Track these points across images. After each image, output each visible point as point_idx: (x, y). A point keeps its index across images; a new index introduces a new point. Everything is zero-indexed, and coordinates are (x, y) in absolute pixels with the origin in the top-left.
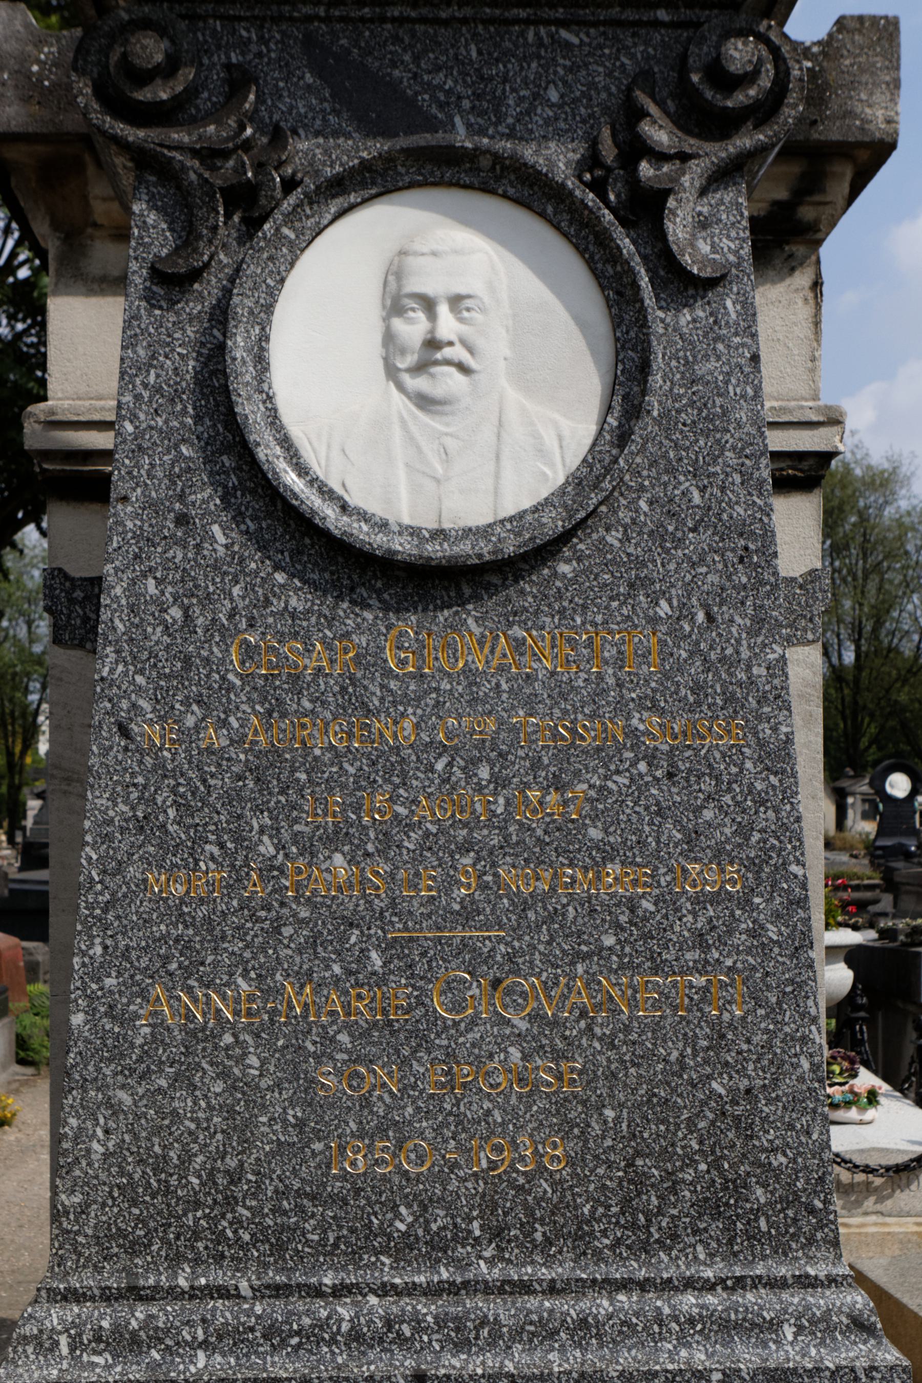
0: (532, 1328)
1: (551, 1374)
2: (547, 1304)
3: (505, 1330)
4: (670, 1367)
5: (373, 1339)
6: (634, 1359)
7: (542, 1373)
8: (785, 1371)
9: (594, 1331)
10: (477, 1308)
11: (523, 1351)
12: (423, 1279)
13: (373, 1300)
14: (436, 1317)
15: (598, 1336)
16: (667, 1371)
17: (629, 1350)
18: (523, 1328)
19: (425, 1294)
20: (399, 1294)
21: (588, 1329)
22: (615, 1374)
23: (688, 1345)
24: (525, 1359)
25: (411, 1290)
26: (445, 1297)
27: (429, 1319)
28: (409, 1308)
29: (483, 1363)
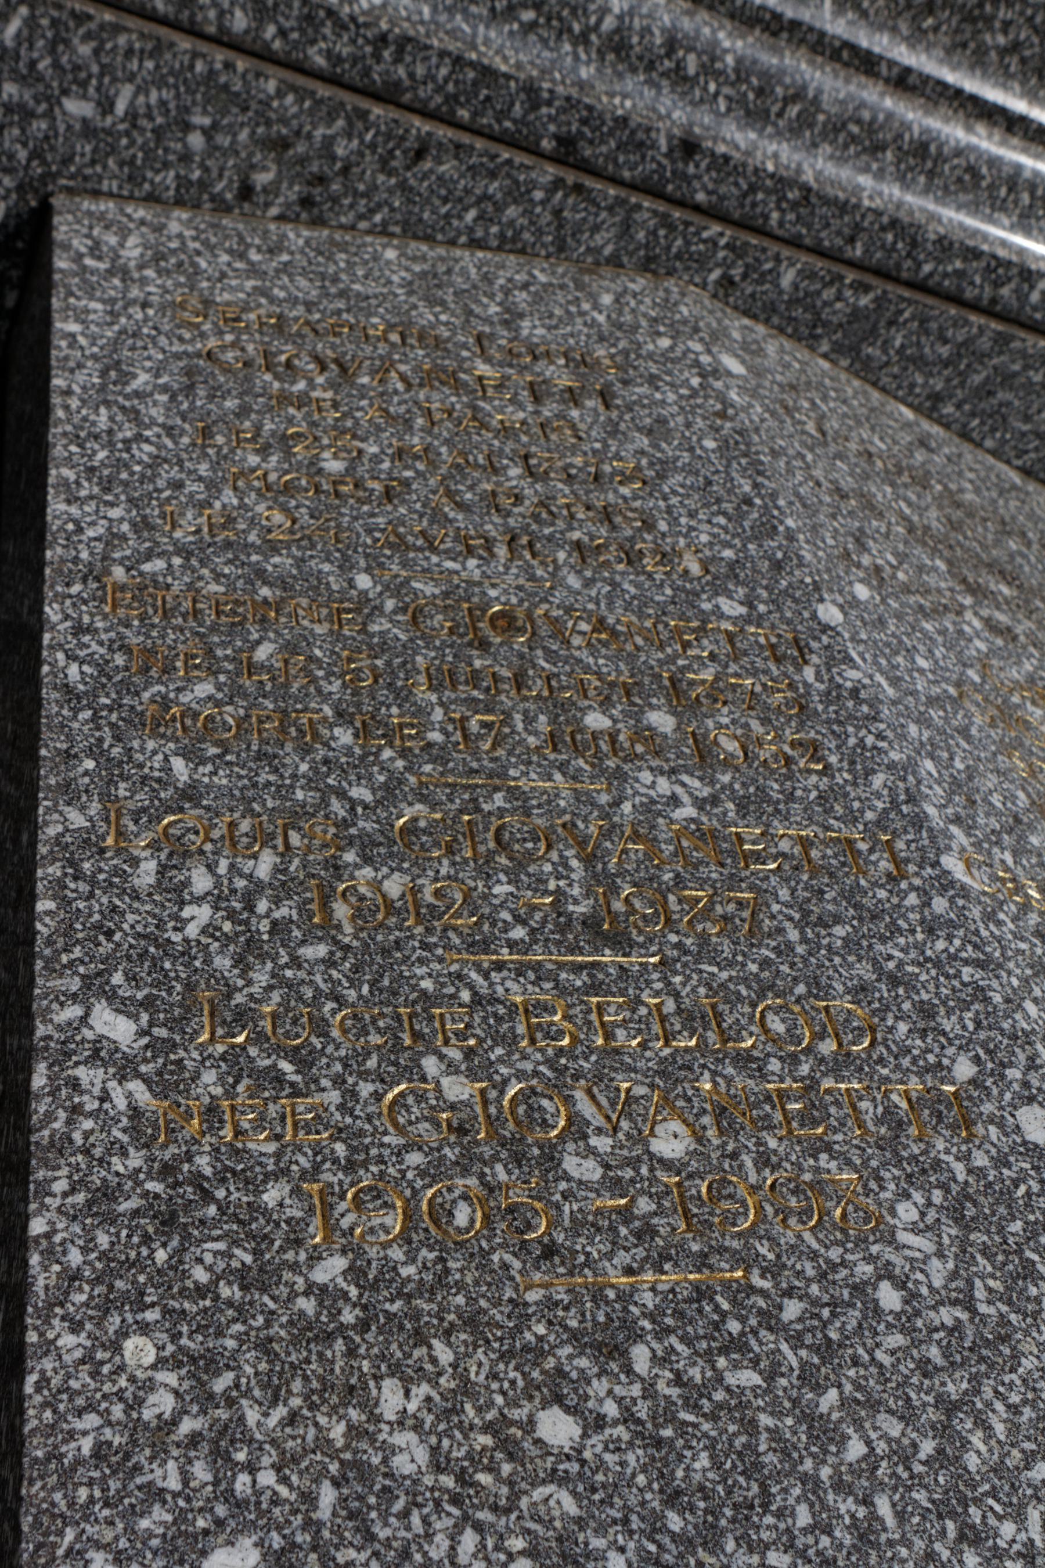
0: (855, 129)
3: (821, 118)
5: (640, 58)
9: (929, 164)
14: (739, 61)
18: (844, 125)
22: (932, 237)
27: (730, 59)
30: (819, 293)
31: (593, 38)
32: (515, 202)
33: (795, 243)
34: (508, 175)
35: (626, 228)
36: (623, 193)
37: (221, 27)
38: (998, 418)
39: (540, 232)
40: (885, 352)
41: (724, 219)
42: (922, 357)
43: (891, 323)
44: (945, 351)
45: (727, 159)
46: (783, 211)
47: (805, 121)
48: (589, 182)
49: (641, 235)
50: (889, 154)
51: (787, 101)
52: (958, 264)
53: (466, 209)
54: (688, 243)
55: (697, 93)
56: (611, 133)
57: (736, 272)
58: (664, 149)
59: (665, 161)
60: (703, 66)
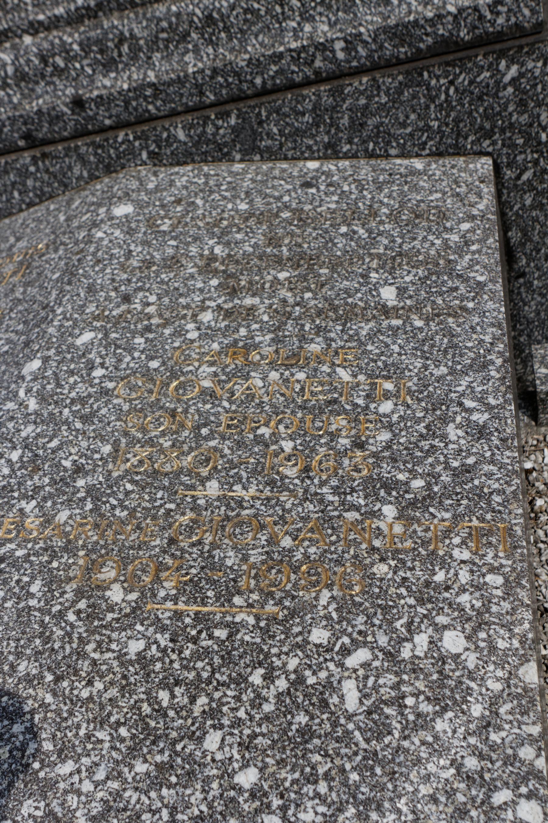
0: (164, 35)
1: (186, 76)
2: (174, 8)
3: (142, 42)
4: (293, 45)
5: (35, 75)
6: (261, 44)
7: (179, 77)
8: (406, 26)
9: (221, 25)
10: (114, 27)
11: (162, 58)
12: (62, 10)
13: (28, 40)
14: (80, 44)
15: (226, 29)
16: (290, 50)
17: (256, 36)
18: (157, 37)
19: (69, 24)
20: (48, 29)
21: (215, 24)
22: (244, 64)
23: (311, 20)
24: (166, 67)
25: (55, 23)
26: (87, 22)
27: (76, 47)
28: (57, 41)
29: (129, 78)
30: (204, 132)
31: (9, 81)
32: (27, 178)
33: (174, 114)
34: (12, 169)
35: (82, 159)
36: (66, 145)
37: (340, 71)
38: (384, 136)
39: (49, 185)
40: (273, 139)
41: (127, 125)
42: (297, 129)
43: (260, 123)
44: (307, 118)
45: (100, 97)
46: (152, 103)
47: (135, 50)
48: (48, 149)
49: (92, 158)
50: (193, 35)
51: (118, 46)
52: (274, 68)
53: (12, 193)
54: (116, 149)
55: (73, 73)
56: (40, 121)
57: (153, 147)
58: (69, 112)
59: (75, 117)
60: (65, 59)
